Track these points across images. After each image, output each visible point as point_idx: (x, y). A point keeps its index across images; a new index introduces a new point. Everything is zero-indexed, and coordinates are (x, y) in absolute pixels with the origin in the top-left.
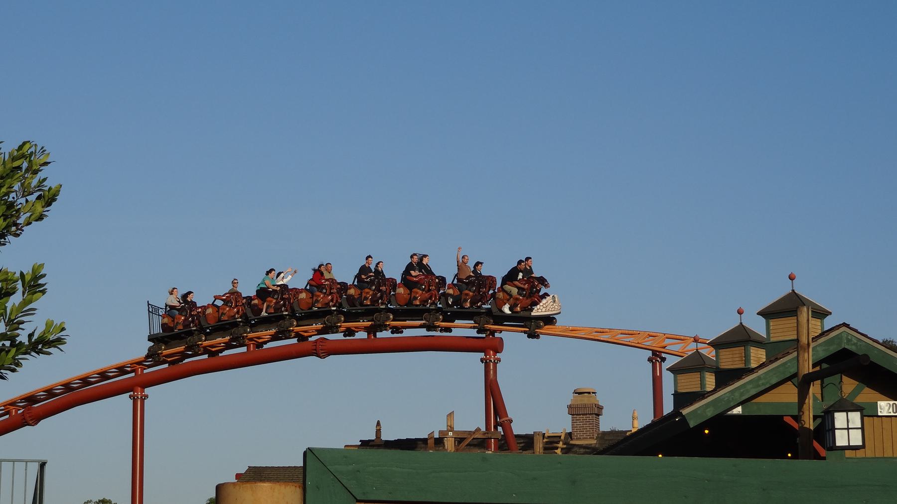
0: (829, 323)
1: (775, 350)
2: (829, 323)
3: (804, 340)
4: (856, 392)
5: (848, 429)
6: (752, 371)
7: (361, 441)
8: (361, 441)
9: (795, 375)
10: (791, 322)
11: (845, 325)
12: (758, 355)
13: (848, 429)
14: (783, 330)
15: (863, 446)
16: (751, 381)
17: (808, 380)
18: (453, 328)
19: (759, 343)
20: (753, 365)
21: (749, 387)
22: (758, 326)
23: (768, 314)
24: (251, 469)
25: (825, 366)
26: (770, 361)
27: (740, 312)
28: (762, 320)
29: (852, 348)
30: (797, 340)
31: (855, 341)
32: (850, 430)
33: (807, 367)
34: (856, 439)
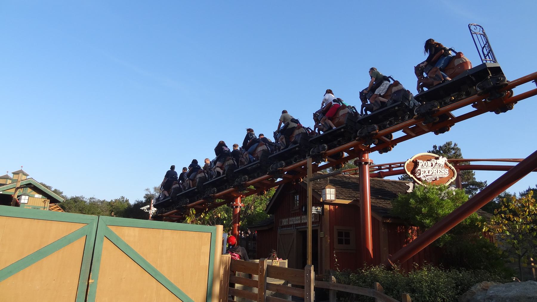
0: (28, 177)
1: (14, 181)
2: (28, 177)
3: (19, 180)
4: (30, 192)
5: (330, 194)
6: (7, 185)
7: (128, 199)
8: (128, 199)
9: (15, 187)
10: (17, 176)
11: (32, 178)
12: (9, 181)
13: (330, 194)
14: (16, 178)
15: (27, 203)
16: (5, 187)
17: (18, 188)
18: (481, 47)
19: (10, 179)
20: (8, 184)
21: (5, 188)
22: (11, 176)
23: (14, 173)
24: (511, 108)
25: (25, 186)
26: (12, 183)
27: (7, 172)
28: (13, 174)
29: (32, 183)
30: (18, 180)
31: (33, 182)
32: (330, 195)
33: (18, 186)
34: (26, 202)
